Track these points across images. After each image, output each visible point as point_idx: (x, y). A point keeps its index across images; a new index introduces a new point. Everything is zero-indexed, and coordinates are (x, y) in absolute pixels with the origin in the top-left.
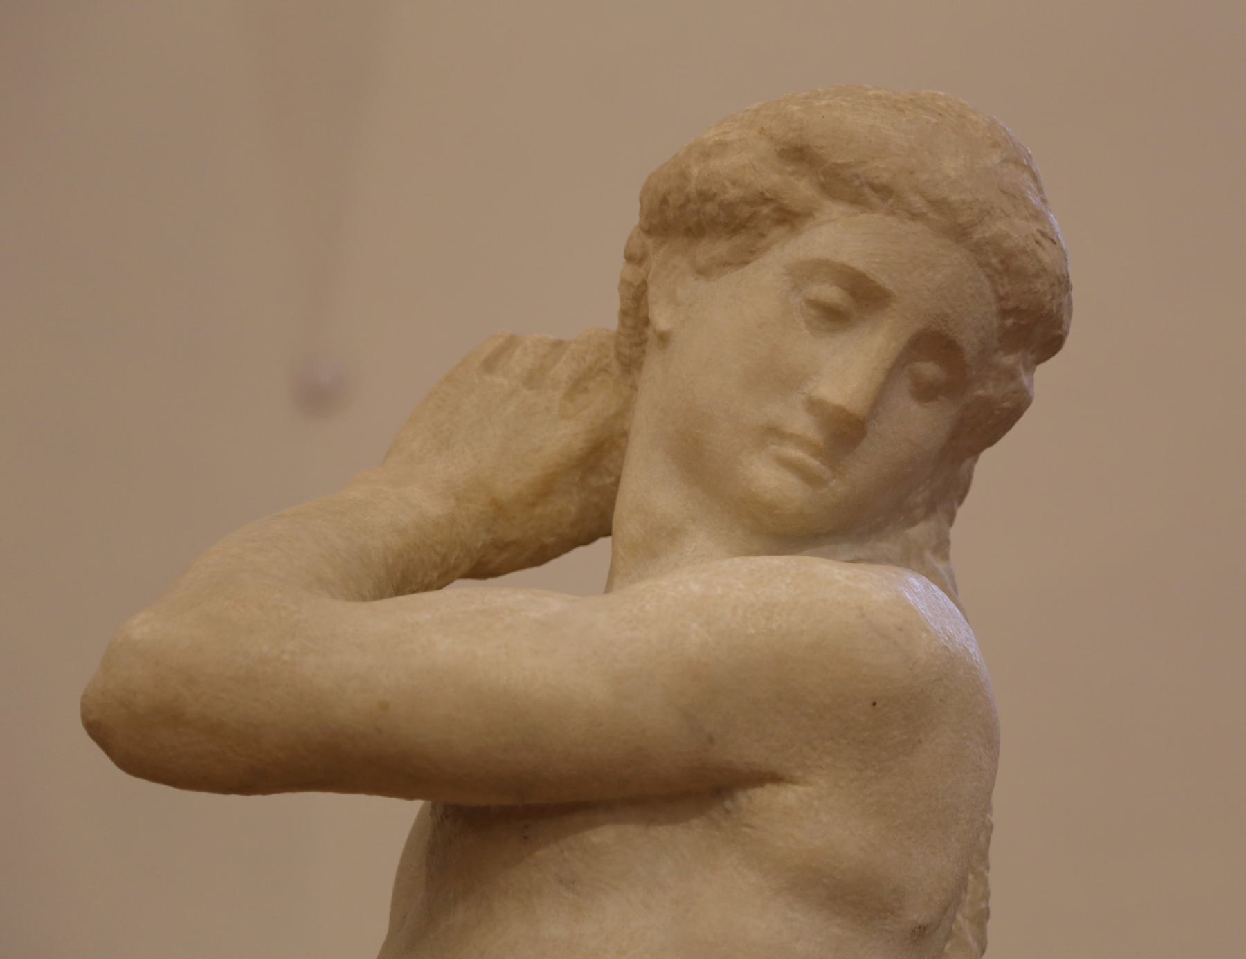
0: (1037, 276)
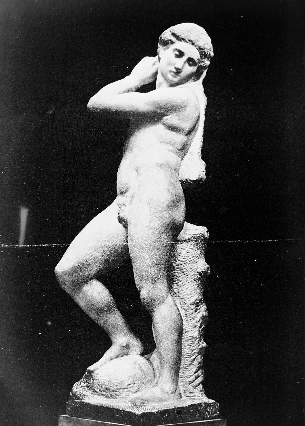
0: (204, 49)
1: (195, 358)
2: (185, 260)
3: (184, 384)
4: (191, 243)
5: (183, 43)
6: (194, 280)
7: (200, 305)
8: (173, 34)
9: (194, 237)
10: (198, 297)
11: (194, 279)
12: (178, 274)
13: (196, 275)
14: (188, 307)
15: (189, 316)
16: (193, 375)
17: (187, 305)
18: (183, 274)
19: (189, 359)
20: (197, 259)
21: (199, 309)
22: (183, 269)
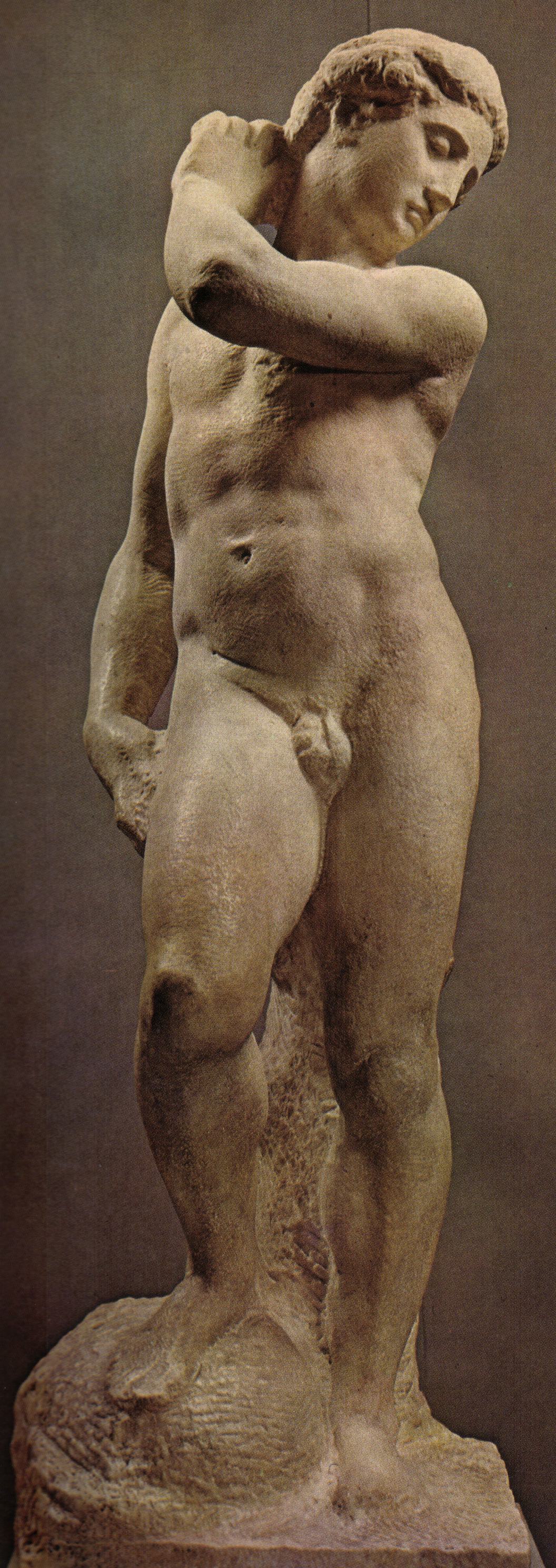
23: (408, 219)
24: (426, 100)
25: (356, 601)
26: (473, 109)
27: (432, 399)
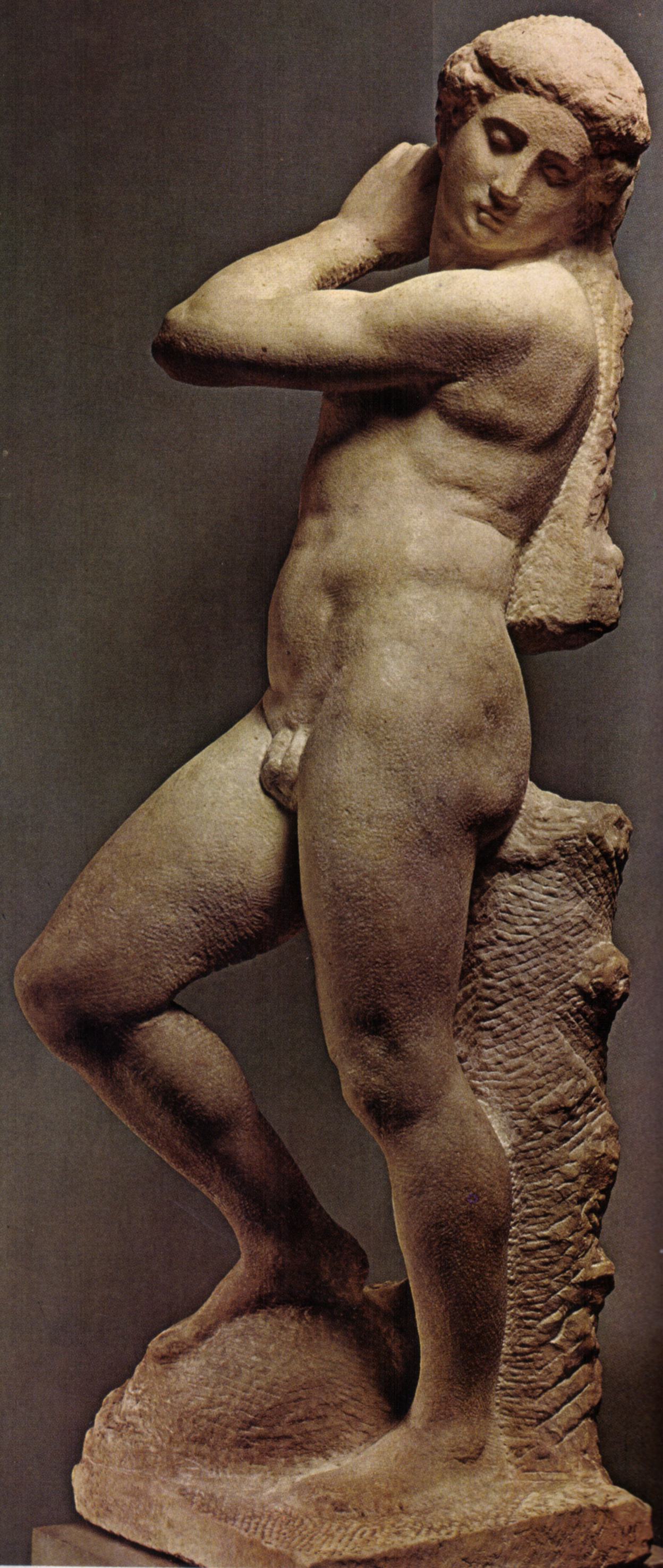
0: (608, 118)
1: (563, 1318)
2: (522, 937)
3: (520, 1420)
4: (550, 872)
5: (522, 98)
6: (558, 1017)
7: (581, 1114)
8: (486, 64)
9: (561, 849)
10: (576, 1083)
11: (558, 1013)
12: (497, 992)
13: (569, 997)
14: (535, 1122)
15: (539, 1156)
16: (550, 1388)
17: (528, 1114)
18: (517, 991)
19: (535, 1322)
20: (574, 935)
21: (579, 1129)
22: (515, 973)
23: (480, 222)
24: (485, 98)
25: (323, 619)
26: (527, 93)
27: (452, 403)
